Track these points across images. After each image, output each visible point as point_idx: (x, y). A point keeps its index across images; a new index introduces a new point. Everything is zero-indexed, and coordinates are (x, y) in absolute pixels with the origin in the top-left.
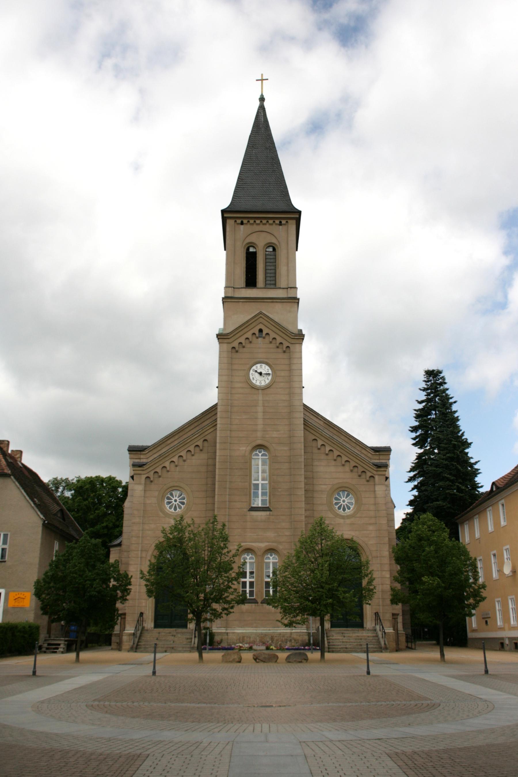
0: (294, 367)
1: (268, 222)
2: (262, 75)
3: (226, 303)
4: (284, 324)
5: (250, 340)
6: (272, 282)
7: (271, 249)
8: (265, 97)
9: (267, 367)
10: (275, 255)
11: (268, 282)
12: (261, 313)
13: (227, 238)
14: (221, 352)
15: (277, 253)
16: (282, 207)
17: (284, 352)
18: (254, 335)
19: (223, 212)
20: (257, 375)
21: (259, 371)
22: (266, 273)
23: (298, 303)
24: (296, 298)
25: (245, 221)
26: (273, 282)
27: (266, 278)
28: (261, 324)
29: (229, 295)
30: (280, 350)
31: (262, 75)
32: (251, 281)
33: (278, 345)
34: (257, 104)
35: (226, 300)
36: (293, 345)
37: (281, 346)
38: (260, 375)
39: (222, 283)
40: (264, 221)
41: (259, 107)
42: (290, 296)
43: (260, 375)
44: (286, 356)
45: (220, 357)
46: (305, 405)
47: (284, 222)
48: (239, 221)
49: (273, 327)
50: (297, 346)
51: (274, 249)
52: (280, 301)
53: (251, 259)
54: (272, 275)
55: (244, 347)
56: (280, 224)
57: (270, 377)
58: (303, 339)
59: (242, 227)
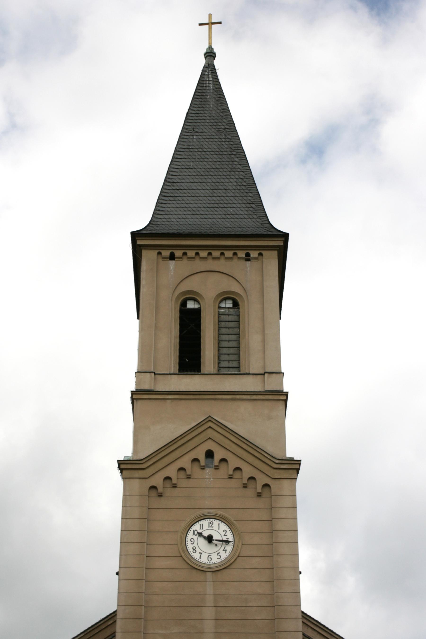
0: (280, 525)
1: (222, 254)
2: (210, 15)
3: (139, 402)
4: (258, 441)
5: (188, 472)
6: (232, 362)
7: (229, 304)
8: (215, 50)
9: (223, 527)
10: (239, 315)
11: (223, 364)
12: (210, 419)
13: (143, 282)
14: (127, 496)
15: (241, 310)
16: (250, 225)
17: (259, 495)
18: (196, 463)
19: (135, 235)
20: (202, 542)
21: (206, 534)
22: (219, 348)
23: (286, 401)
24: (282, 392)
25: (178, 253)
26: (235, 364)
27: (219, 357)
28: (210, 441)
29: (146, 387)
30: (250, 492)
31: (210, 15)
32: (189, 360)
33: (245, 481)
34: (202, 62)
35: (137, 396)
36: (277, 482)
37: (251, 484)
38: (208, 544)
39: (132, 364)
40: (216, 253)
41: (205, 67)
42: (268, 388)
43: (208, 544)
44: (261, 503)
45: (124, 507)
46: (303, 612)
47: (254, 254)
48: (166, 253)
49: (234, 446)
50: (286, 483)
51: (236, 304)
52: (248, 397)
53: (189, 323)
54: (231, 351)
55: (174, 486)
56: (248, 258)
57: (229, 548)
58: (298, 470)
59: (172, 263)
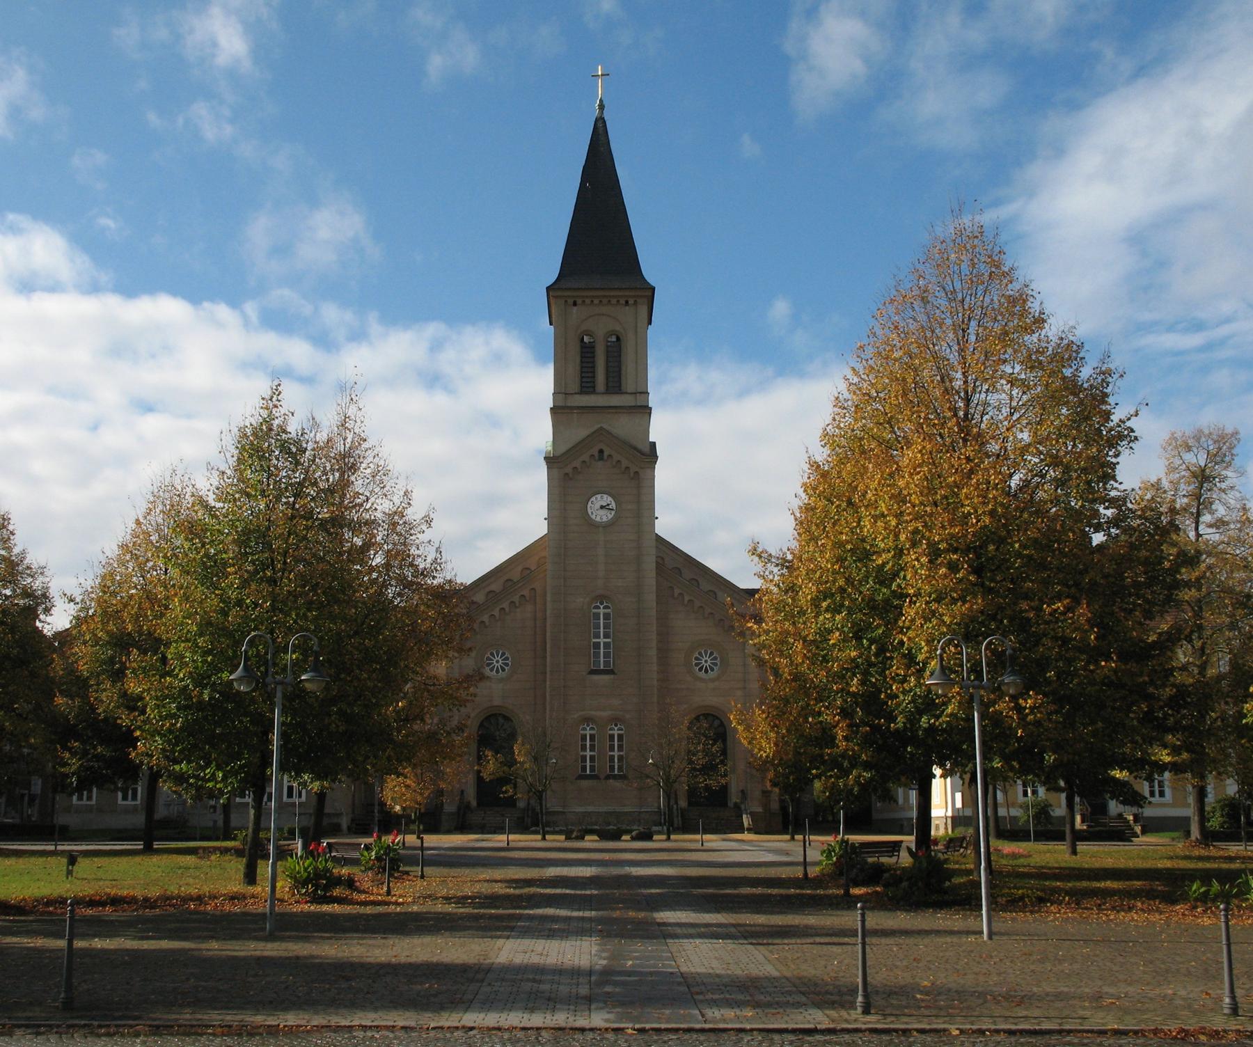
6: (615, 384)
7: (614, 339)
12: (601, 428)
25: (579, 301)
32: (587, 386)
35: (555, 411)
38: (600, 508)
43: (600, 508)
46: (659, 538)
51: (618, 339)
53: (587, 352)
59: (600, 463)
